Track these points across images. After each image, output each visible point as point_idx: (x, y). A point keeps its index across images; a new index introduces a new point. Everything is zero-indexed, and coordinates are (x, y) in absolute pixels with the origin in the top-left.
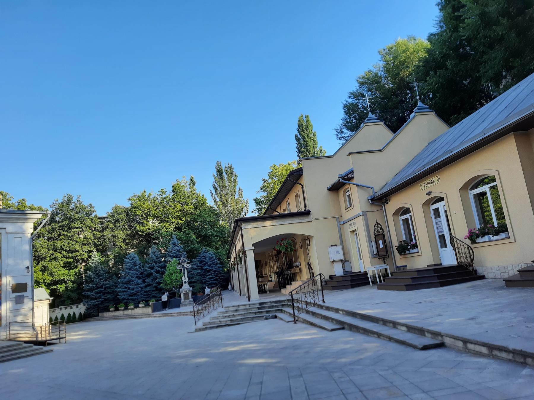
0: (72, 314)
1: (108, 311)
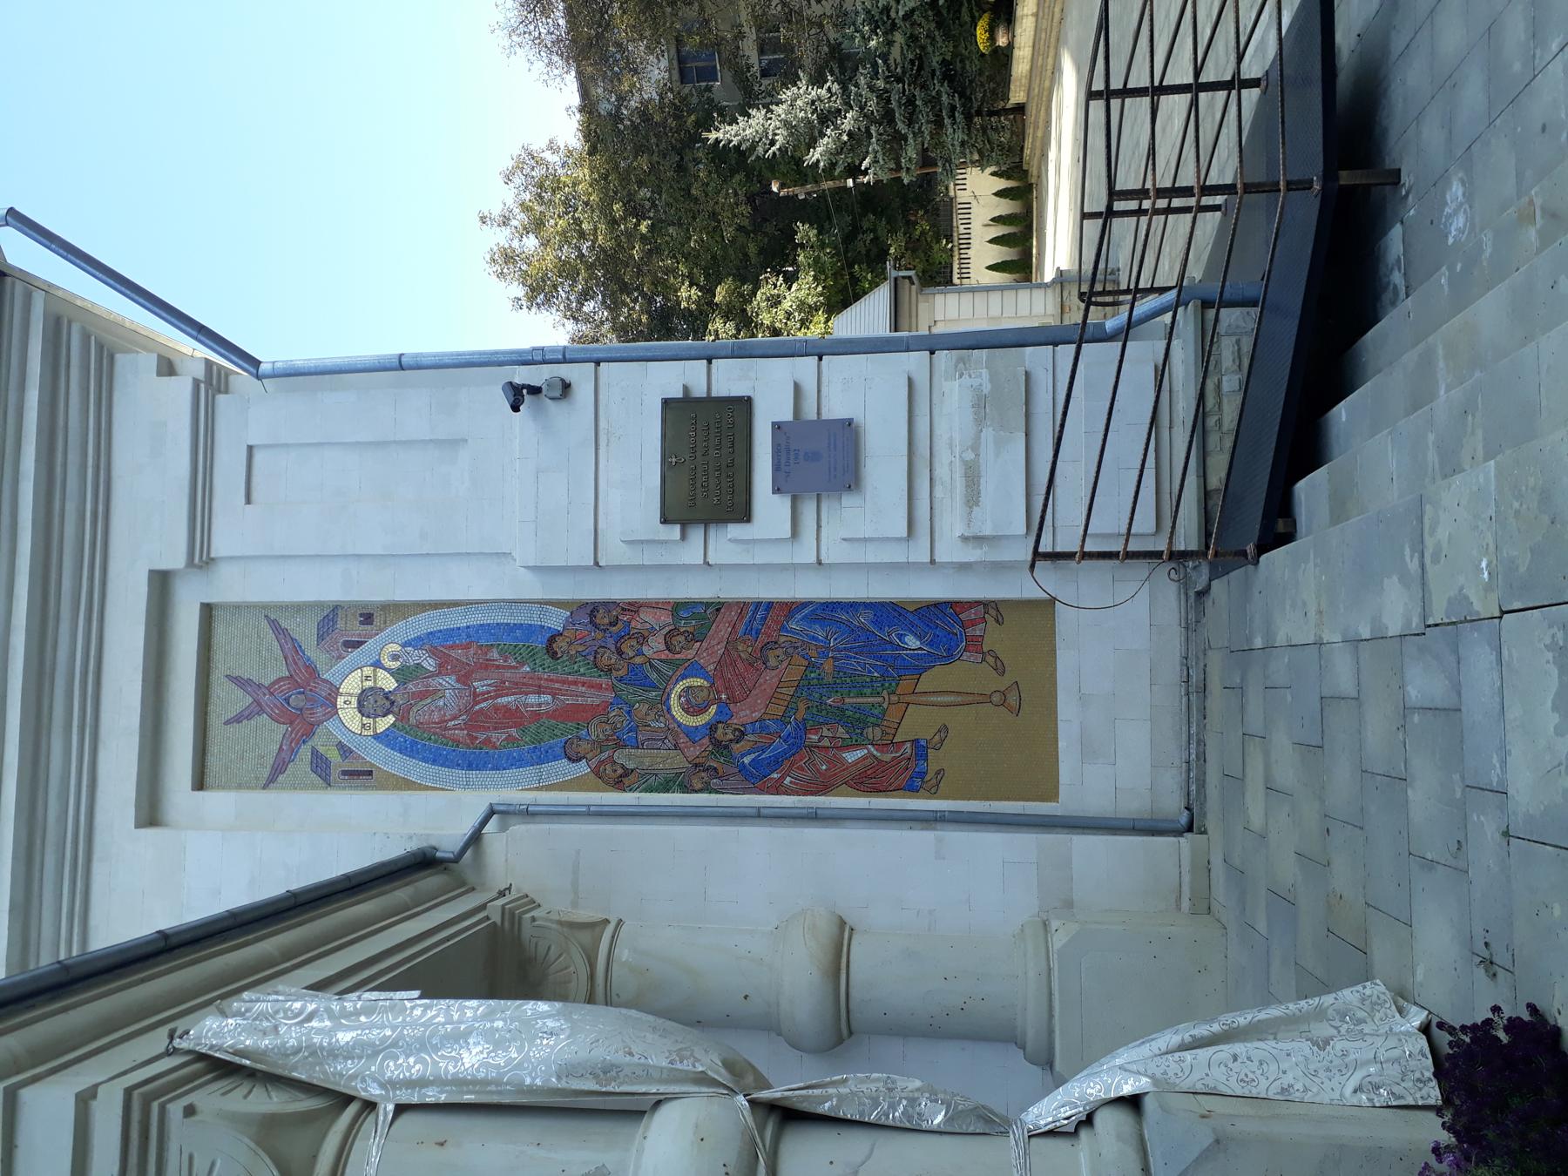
1: (1003, 58)
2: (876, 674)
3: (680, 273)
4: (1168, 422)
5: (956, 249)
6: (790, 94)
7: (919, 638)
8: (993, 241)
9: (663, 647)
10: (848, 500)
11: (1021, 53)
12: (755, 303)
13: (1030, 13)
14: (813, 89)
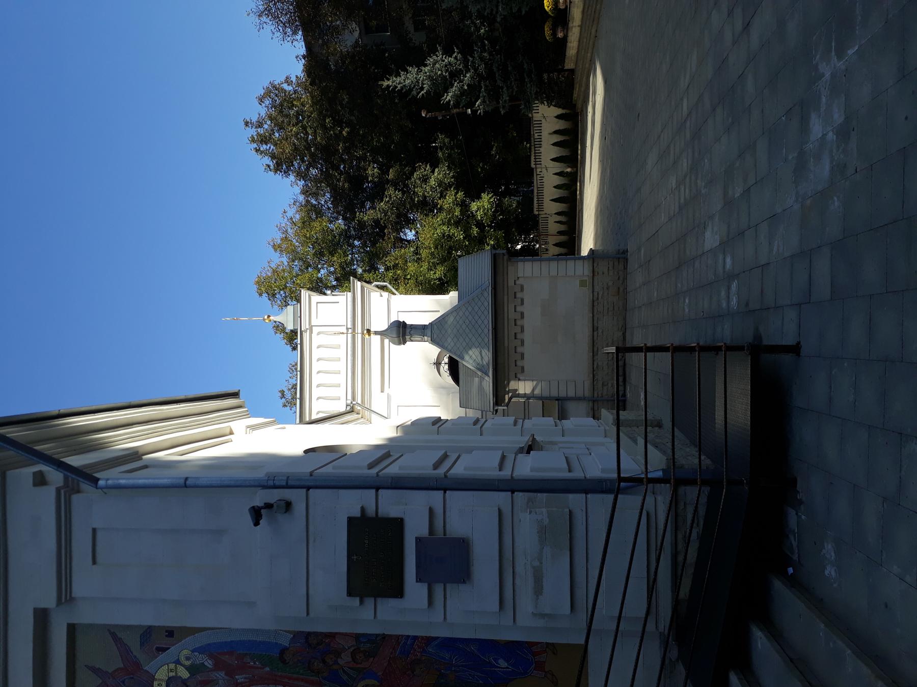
0: (557, 138)
1: (562, 44)
2: (481, 682)
3: (368, 159)
4: (655, 547)
5: (533, 147)
6: (432, 60)
7: (507, 661)
8: (555, 144)
9: (350, 659)
10: (462, 587)
11: (572, 45)
12: (413, 179)
13: (577, 25)
14: (445, 58)
